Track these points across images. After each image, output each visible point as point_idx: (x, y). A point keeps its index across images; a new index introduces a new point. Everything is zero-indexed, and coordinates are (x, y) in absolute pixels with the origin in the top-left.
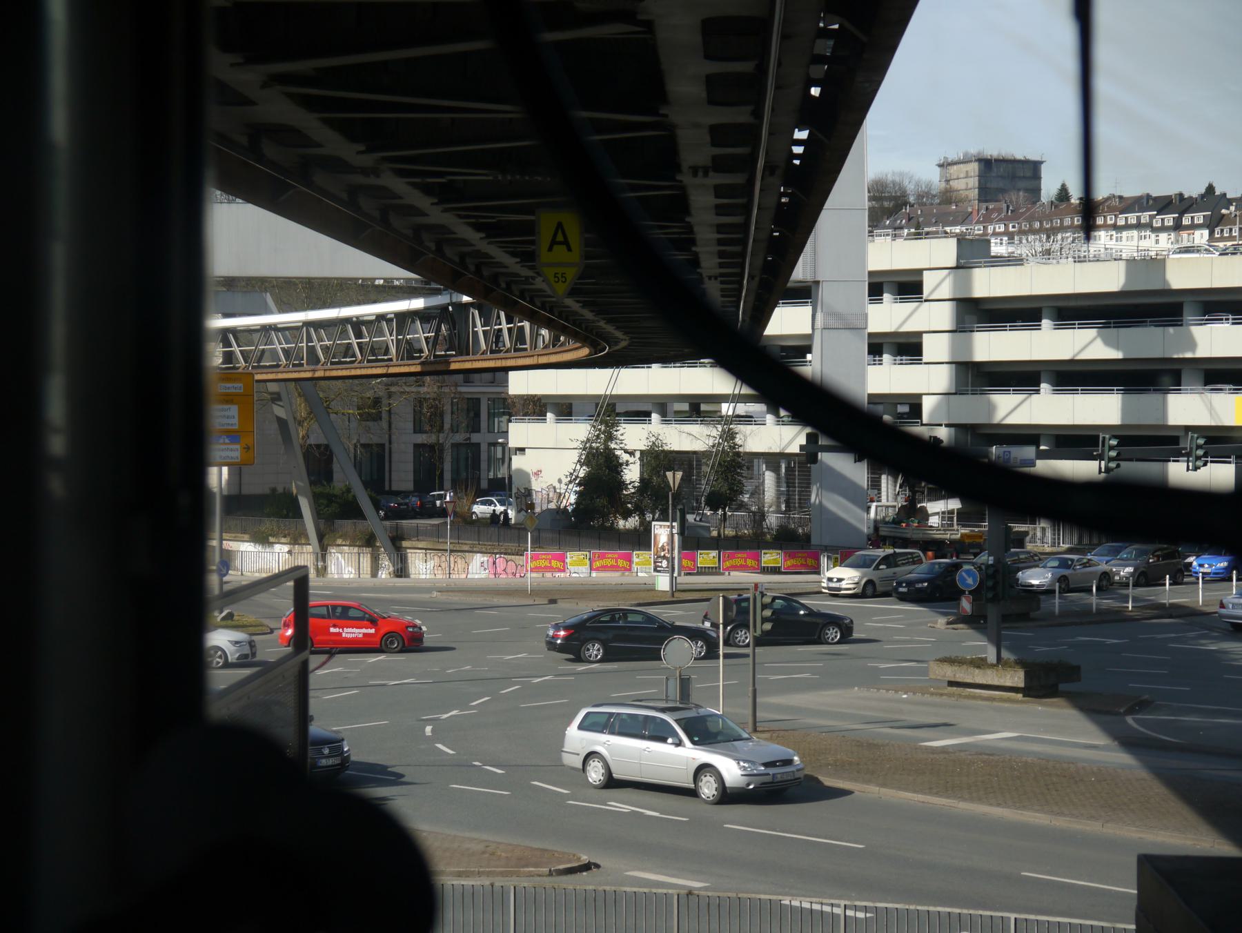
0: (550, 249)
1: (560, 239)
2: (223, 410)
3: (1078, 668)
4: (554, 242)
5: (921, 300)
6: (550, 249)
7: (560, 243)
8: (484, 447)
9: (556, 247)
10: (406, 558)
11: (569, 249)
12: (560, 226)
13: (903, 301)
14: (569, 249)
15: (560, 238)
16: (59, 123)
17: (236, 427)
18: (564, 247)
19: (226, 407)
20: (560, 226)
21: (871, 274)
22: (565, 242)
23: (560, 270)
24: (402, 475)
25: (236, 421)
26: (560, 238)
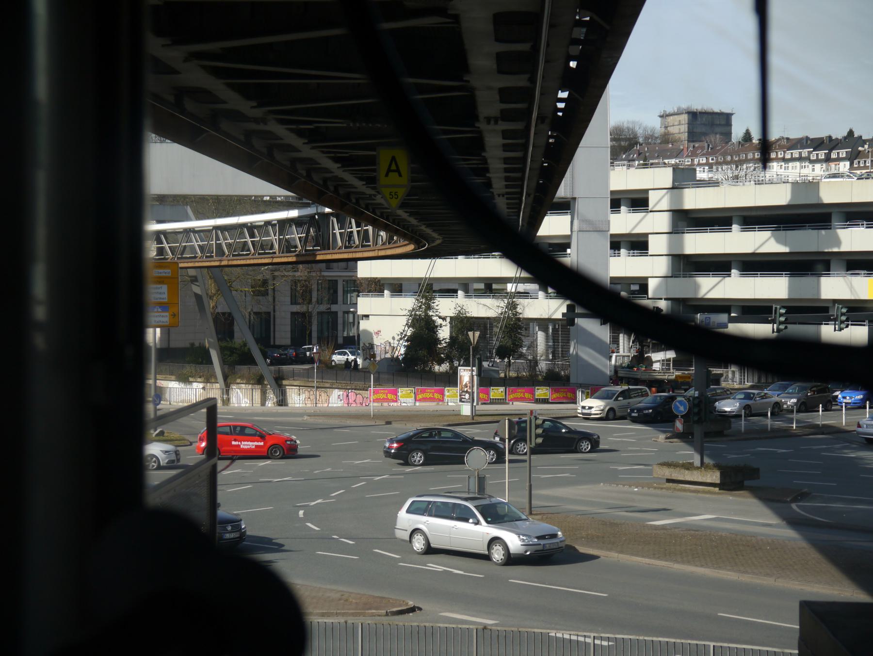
0: (387, 175)
1: (393, 168)
2: (157, 288)
3: (758, 470)
4: (389, 170)
5: (647, 211)
6: (387, 175)
7: (394, 171)
8: (340, 315)
9: (391, 174)
10: (285, 392)
11: (400, 175)
12: (394, 159)
13: (635, 211)
14: (400, 175)
15: (394, 167)
16: (42, 86)
17: (166, 300)
18: (396, 174)
19: (159, 286)
20: (394, 159)
21: (612, 192)
22: (397, 170)
23: (394, 190)
24: (283, 334)
25: (166, 296)
26: (394, 167)
